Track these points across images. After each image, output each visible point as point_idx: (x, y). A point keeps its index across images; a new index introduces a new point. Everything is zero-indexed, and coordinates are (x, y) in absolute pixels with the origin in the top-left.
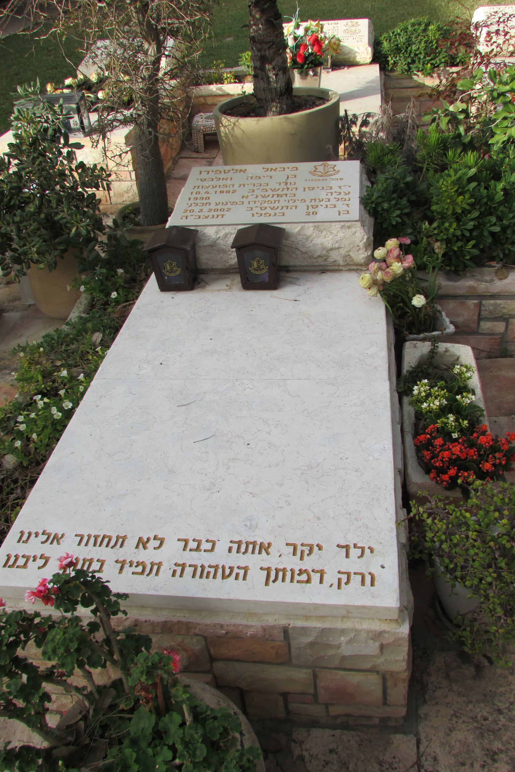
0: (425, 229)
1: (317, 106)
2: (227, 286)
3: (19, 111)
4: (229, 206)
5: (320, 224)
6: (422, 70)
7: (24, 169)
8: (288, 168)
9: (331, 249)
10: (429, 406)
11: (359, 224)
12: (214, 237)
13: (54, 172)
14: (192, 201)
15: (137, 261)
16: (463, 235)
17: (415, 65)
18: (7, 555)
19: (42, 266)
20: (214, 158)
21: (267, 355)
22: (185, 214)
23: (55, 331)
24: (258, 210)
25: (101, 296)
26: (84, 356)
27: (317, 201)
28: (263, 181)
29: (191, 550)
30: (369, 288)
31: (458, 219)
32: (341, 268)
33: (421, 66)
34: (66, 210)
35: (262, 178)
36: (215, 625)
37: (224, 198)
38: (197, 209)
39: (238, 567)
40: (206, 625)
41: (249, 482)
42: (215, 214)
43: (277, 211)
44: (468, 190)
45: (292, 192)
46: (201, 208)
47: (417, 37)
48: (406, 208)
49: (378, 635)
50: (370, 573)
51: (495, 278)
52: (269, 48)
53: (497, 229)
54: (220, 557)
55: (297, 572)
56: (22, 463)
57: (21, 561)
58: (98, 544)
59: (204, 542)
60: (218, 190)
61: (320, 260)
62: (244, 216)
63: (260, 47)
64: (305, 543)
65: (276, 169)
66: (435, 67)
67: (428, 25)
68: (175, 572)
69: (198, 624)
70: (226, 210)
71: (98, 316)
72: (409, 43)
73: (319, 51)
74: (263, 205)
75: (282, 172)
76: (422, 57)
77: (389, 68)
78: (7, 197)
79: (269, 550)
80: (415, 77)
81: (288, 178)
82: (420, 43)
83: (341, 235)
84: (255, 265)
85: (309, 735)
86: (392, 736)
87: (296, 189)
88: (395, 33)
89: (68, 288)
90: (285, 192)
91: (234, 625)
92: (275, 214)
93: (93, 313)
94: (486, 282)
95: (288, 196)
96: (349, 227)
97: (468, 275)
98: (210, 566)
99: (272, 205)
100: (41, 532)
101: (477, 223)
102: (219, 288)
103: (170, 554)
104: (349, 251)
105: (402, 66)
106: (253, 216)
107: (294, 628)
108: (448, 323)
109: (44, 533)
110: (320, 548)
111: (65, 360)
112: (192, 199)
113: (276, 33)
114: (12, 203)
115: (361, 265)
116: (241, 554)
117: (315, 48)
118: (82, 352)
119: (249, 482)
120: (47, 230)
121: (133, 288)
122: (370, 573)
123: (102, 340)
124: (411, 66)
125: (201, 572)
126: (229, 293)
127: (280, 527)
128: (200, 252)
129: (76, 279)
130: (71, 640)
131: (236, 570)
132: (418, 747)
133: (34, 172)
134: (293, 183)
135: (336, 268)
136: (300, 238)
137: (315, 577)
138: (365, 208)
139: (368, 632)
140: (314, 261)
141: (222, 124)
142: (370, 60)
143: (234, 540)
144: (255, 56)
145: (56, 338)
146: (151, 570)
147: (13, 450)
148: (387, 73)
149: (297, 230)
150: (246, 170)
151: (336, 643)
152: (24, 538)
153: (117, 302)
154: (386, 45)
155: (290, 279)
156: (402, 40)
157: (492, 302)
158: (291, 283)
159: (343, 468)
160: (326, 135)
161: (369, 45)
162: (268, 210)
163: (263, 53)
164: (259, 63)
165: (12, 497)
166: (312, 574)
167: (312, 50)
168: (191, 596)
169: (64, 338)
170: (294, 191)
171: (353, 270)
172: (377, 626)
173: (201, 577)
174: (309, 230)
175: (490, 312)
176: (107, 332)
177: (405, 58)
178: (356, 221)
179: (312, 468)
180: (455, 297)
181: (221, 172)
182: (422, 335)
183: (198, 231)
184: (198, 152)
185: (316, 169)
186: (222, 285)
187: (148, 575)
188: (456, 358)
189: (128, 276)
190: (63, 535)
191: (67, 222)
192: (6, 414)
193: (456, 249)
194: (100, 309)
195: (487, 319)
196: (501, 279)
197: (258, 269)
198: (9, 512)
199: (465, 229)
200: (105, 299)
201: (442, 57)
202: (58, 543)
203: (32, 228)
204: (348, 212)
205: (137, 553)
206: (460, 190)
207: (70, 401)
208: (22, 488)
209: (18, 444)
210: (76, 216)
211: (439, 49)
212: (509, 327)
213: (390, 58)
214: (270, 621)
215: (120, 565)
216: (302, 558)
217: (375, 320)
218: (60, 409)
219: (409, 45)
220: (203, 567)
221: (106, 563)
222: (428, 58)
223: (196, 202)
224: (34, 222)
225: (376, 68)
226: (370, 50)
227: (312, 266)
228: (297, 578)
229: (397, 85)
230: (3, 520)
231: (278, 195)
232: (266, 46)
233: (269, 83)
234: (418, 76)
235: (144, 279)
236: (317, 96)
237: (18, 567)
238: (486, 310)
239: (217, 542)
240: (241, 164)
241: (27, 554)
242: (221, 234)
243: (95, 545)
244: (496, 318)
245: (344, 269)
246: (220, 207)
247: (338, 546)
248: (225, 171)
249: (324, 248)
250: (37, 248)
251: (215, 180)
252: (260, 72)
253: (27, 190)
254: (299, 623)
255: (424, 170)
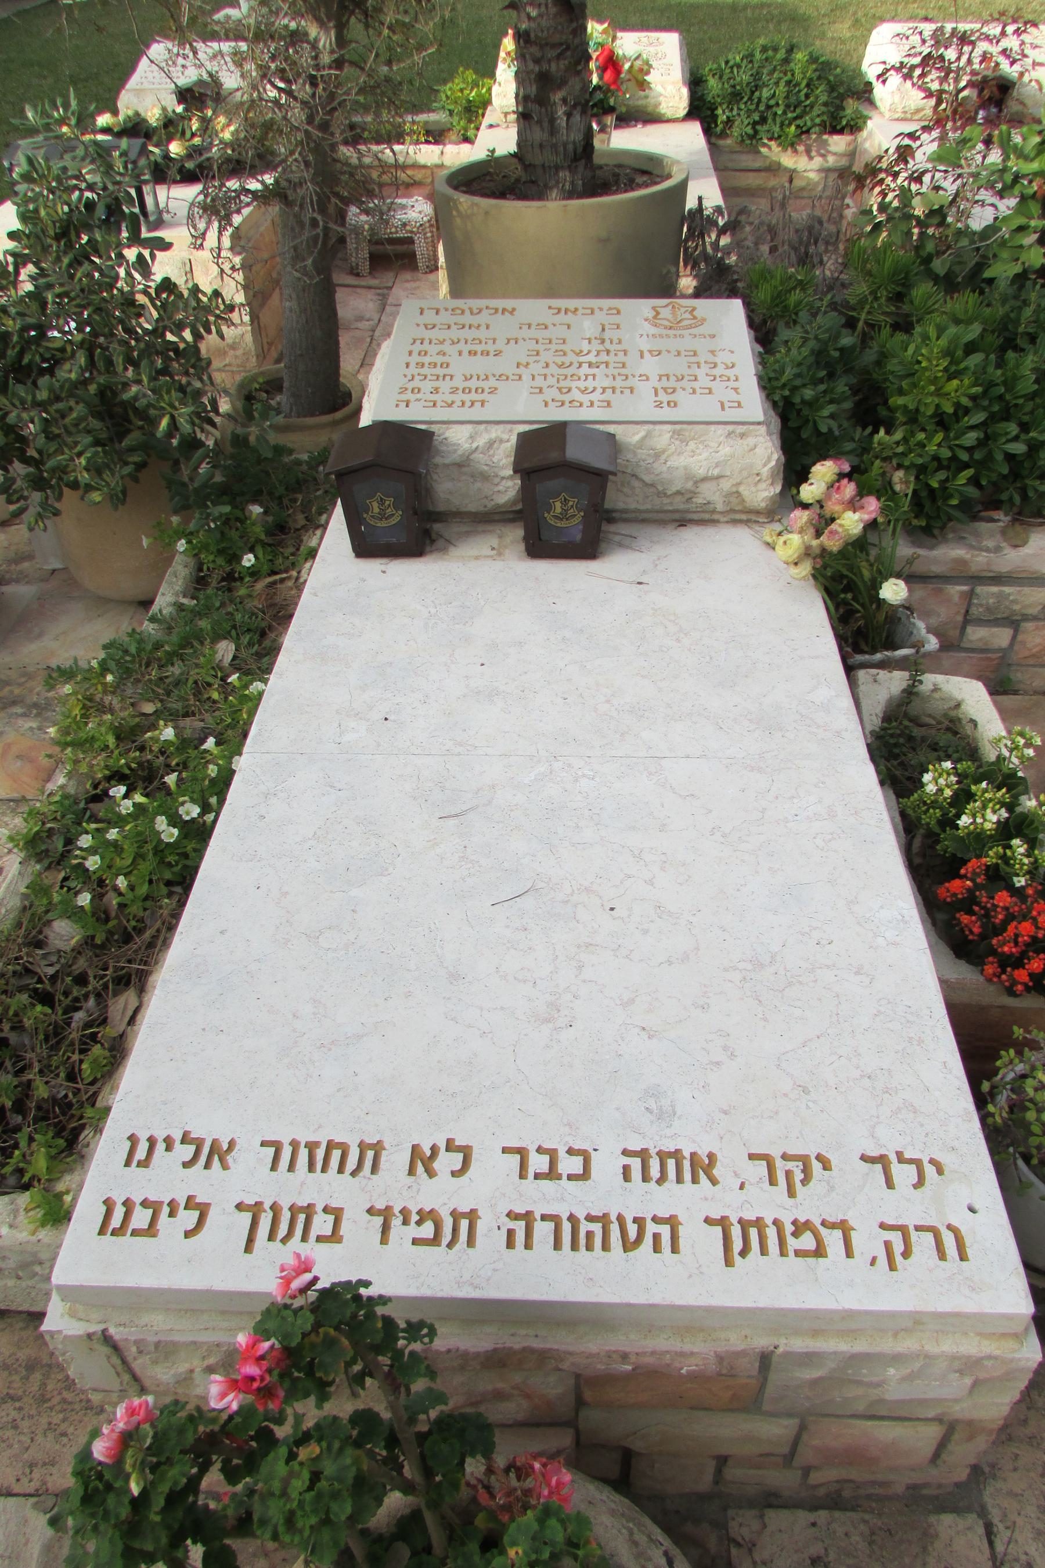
0: (879, 444)
1: (640, 186)
2: (493, 549)
3: (30, 161)
4: (492, 382)
5: (685, 426)
6: (779, 137)
7: (50, 286)
8: (601, 309)
9: (705, 479)
10: (974, 822)
11: (763, 429)
12: (466, 446)
13: (113, 296)
14: (413, 370)
15: (287, 489)
16: (954, 458)
17: (765, 128)
18: (105, 1202)
19: (96, 496)
20: (391, 288)
21: (608, 701)
22: (404, 397)
23: (130, 635)
24: (554, 393)
25: (220, 561)
26: (200, 693)
27: (673, 378)
28: (553, 333)
29: (537, 1176)
30: (796, 564)
32: (716, 517)
33: (777, 129)
34: (145, 379)
35: (551, 327)
36: (609, 1355)
37: (479, 365)
38: (427, 386)
39: (655, 1219)
40: (590, 1356)
41: (632, 1001)
42: (467, 398)
43: (593, 397)
44: (966, 368)
45: (617, 359)
46: (436, 384)
47: (771, 73)
48: (846, 399)
49: (968, 1365)
50: (949, 1227)
51: (1004, 544)
52: (559, 57)
53: (1019, 448)
54: (607, 1193)
55: (789, 1228)
56: (93, 937)
57: (141, 1218)
58: (319, 1166)
59: (562, 1153)
60: (466, 349)
61: (678, 499)
62: (528, 406)
63: (538, 55)
64: (791, 1152)
65: (576, 309)
66: (804, 131)
68: (511, 1233)
69: (571, 1353)
70: (487, 390)
71: (218, 604)
73: (615, 82)
74: (563, 384)
75: (588, 319)
76: (779, 112)
77: (718, 130)
78: (14, 347)
79: (715, 1172)
80: (764, 150)
81: (603, 330)
82: (777, 84)
83: (726, 450)
84: (558, 507)
85: (765, 1526)
86: (932, 1519)
87: (625, 352)
88: (731, 63)
89: (145, 542)
90: (604, 357)
91: (653, 1353)
92: (592, 404)
93: (207, 597)
94: (988, 550)
95: (611, 366)
96: (742, 436)
97: (950, 536)
98: (590, 1218)
99: (582, 384)
100: (178, 1136)
101: (982, 435)
102: (474, 552)
103: (490, 1188)
104: (739, 484)
105: (741, 127)
106: (546, 405)
107: (787, 1354)
108: (924, 631)
109: (185, 1139)
110: (826, 1165)
111: (161, 701)
112: (412, 365)
113: (574, 25)
114: (26, 361)
115: (758, 513)
116: (653, 1183)
117: (608, 75)
118: (196, 682)
119: (632, 1001)
120: (102, 420)
121: (280, 543)
122: (949, 1227)
123: (235, 658)
124: (758, 127)
125: (574, 1234)
126: (499, 564)
127: (726, 1113)
128: (435, 477)
129: (159, 524)
130: (335, 1496)
131: (651, 1228)
132: (991, 1543)
133: (73, 294)
134: (615, 341)
135: (707, 516)
136: (642, 453)
137: (833, 1239)
138: (768, 396)
139: (954, 1358)
140: (666, 501)
141: (458, 210)
142: (685, 112)
143: (631, 1148)
144: (528, 73)
145: (133, 650)
146: (455, 1230)
147: (75, 914)
148: (713, 140)
149: (637, 438)
150: (514, 309)
151: (875, 1379)
152: (140, 1153)
153: (254, 573)
154: (713, 84)
155: (617, 538)
156: (744, 77)
157: (994, 589)
158: (621, 545)
159: (828, 967)
161: (684, 83)
162: (575, 394)
163: (545, 67)
164: (534, 88)
165: (79, 1016)
166: (823, 1231)
167: (601, 78)
168: (562, 1299)
169: (151, 652)
170: (621, 357)
171: (740, 521)
172: (971, 1347)
173: (574, 1246)
174: (662, 438)
175: (988, 609)
176: (245, 639)
177: (749, 113)
178: (759, 423)
179: (762, 966)
181: (463, 312)
182: (878, 656)
183: (433, 434)
184: (358, 275)
185: (658, 313)
186: (481, 545)
187: (450, 1245)
188: (952, 704)
189: (270, 519)
190: (232, 1144)
191: (150, 405)
192: (44, 823)
193: (935, 485)
194: (218, 589)
195: (980, 622)
196: (1016, 546)
197: (564, 516)
198: (76, 1057)
199: (957, 446)
200: (228, 569)
201: (815, 116)
202: (225, 1166)
203: (74, 415)
204: (739, 406)
205: (415, 1187)
206: (953, 368)
207: (193, 801)
208: (98, 995)
209: (85, 899)
210: (168, 392)
211: (812, 99)
212: (1020, 638)
213: (719, 111)
214: (735, 1341)
215: (379, 1220)
216: (791, 1193)
218: (174, 820)
219: (756, 86)
220: (572, 1218)
221: (345, 1217)
222: (790, 115)
223: (423, 371)
224: (77, 403)
226: (685, 91)
227: (658, 512)
228: (792, 1243)
229: (730, 165)
230: (62, 1075)
231: (590, 365)
232: (552, 53)
233: (553, 131)
234: (770, 148)
235: (303, 527)
236: (637, 167)
237: (135, 1233)
238: (981, 605)
239: (593, 1153)
240: (504, 296)
241: (152, 1198)
242: (481, 441)
243: (311, 1167)
244: (997, 619)
245: (723, 519)
246: (473, 384)
247: (864, 1158)
248: (471, 309)
249: (689, 477)
250: (89, 460)
251: (453, 327)
252: (535, 107)
253: (56, 334)
254: (799, 1344)
255: (861, 324)
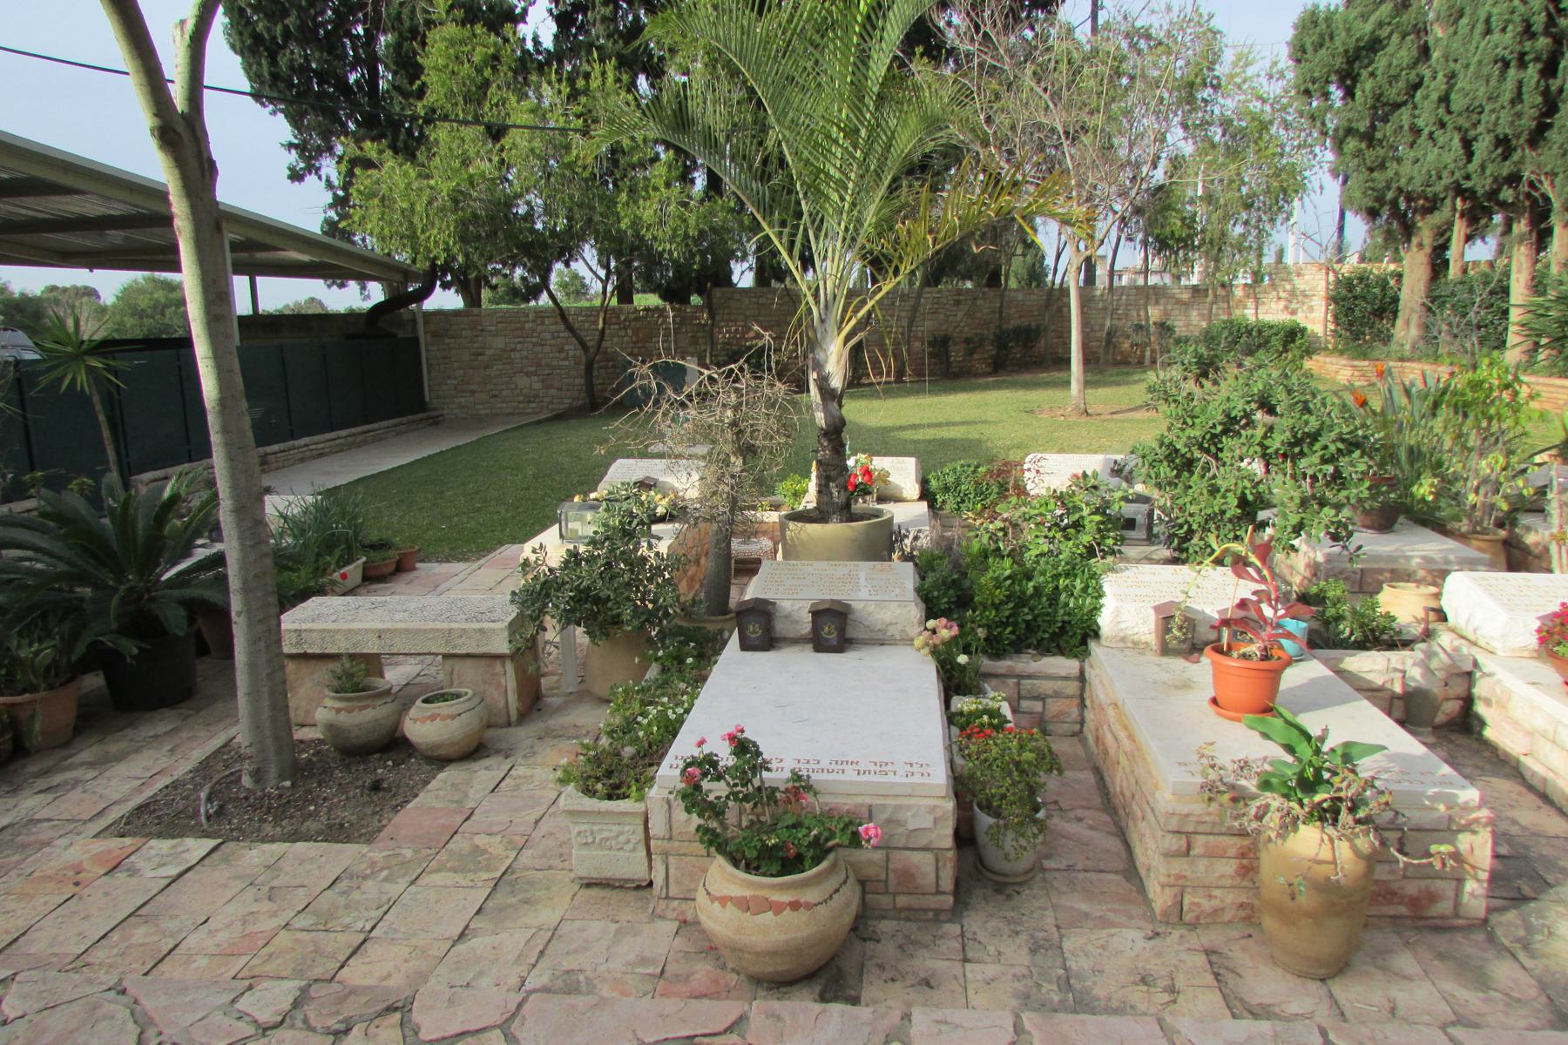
31: (997, 609)
49: (933, 809)
67: (977, 467)
72: (958, 483)
105: (951, 504)
154: (934, 484)
156: (950, 479)
160: (882, 543)
174: (872, 607)
180: (996, 676)
195: (1026, 698)
197: (829, 633)
217: (927, 677)
225: (925, 504)
